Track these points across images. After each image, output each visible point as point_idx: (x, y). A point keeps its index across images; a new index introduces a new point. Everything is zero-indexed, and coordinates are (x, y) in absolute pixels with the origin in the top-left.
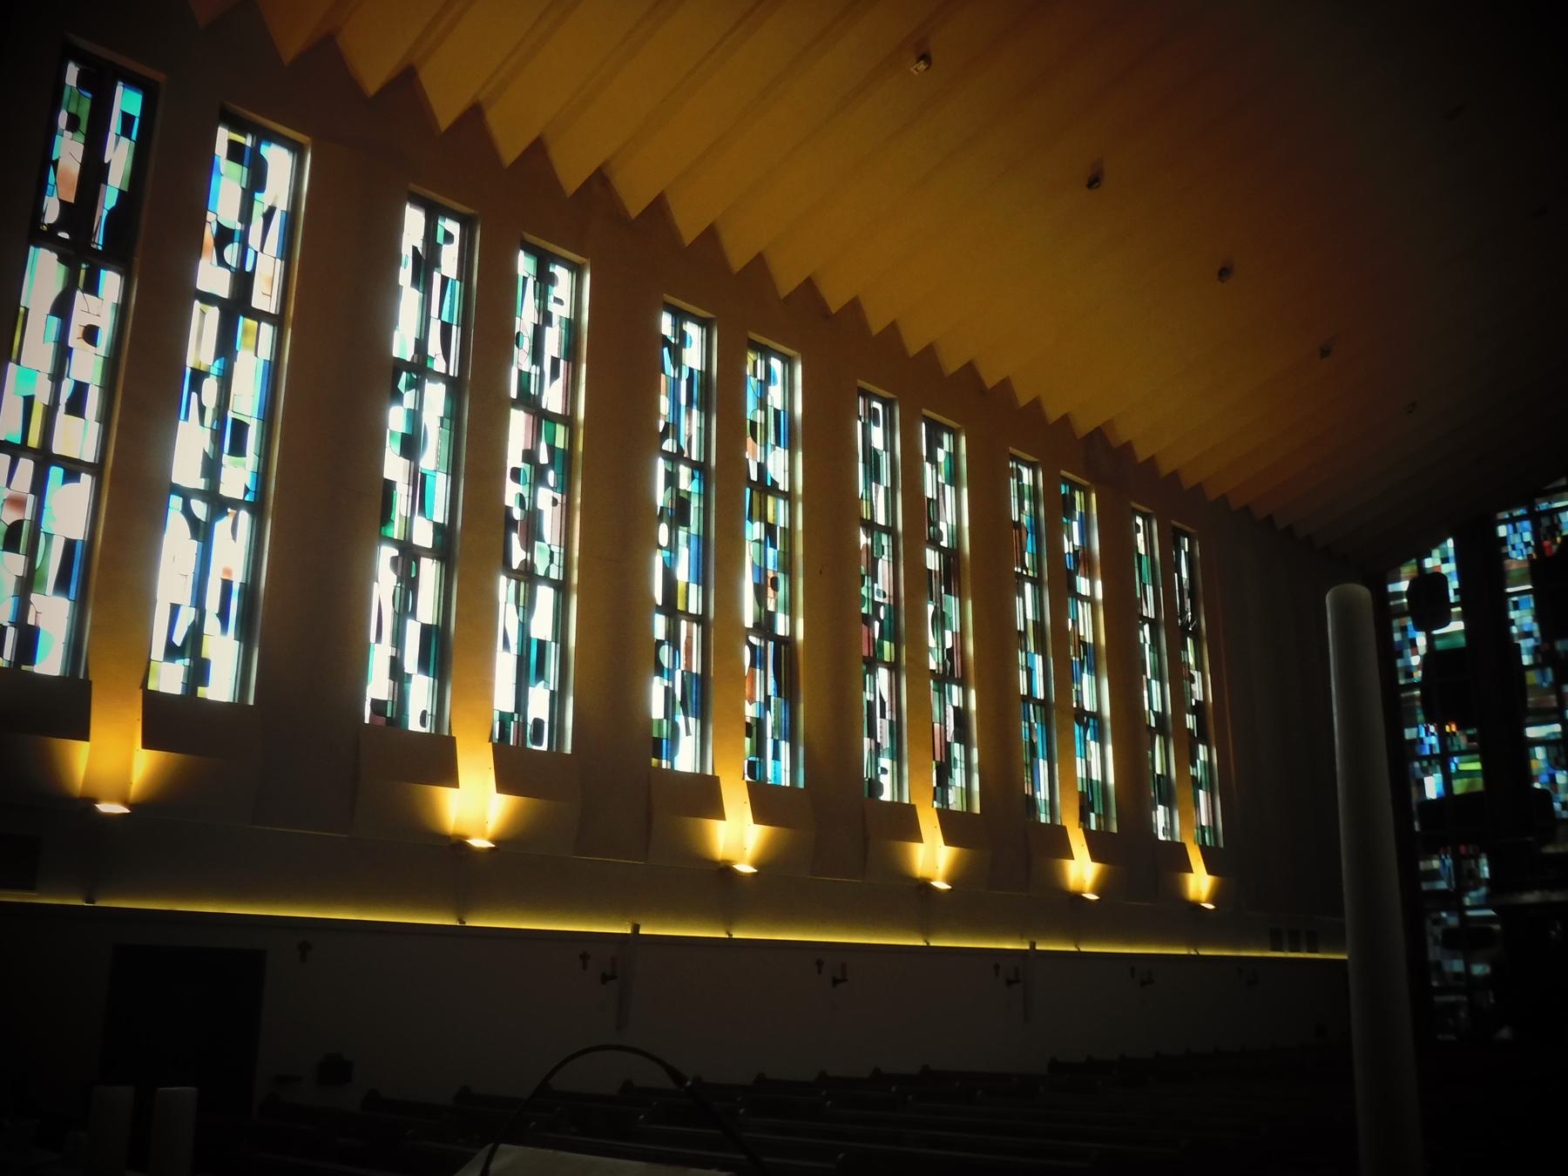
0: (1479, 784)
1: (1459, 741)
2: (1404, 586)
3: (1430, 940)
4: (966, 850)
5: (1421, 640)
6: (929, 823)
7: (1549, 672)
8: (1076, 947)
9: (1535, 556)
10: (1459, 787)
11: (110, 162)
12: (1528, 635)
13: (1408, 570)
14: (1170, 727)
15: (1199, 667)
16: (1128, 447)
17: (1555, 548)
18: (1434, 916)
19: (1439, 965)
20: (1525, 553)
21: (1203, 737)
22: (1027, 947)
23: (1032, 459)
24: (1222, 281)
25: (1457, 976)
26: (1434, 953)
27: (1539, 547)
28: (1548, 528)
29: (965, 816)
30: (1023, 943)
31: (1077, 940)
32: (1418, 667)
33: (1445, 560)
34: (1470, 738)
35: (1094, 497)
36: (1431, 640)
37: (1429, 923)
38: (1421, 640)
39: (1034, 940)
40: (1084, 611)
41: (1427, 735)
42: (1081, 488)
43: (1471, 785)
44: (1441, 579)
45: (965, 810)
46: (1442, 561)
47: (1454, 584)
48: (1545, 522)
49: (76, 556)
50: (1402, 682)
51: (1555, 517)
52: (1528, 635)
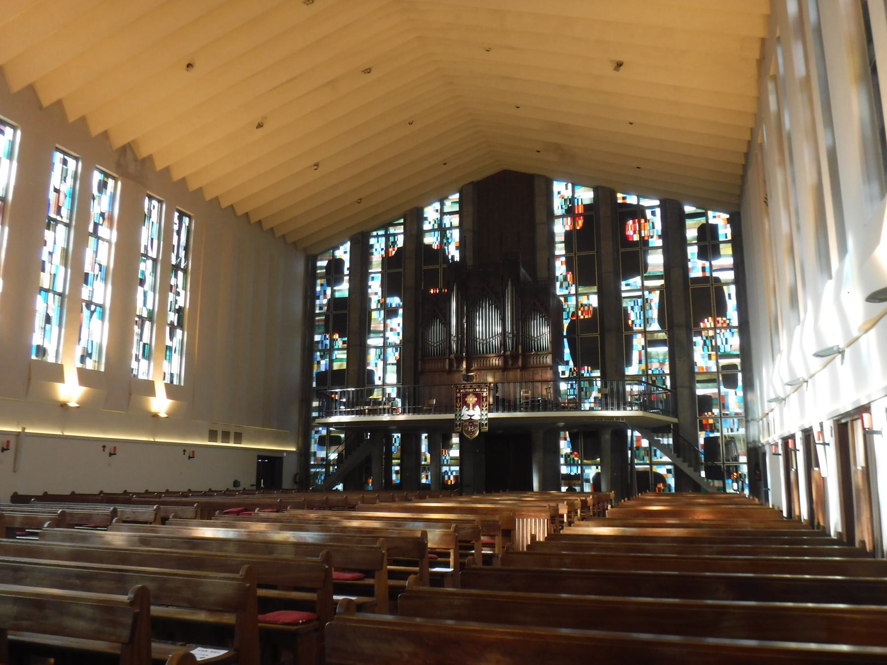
0: (344, 367)
1: (338, 343)
2: (324, 263)
3: (313, 441)
4: (179, 402)
5: (329, 291)
6: (160, 388)
7: (382, 312)
8: (62, 432)
9: (384, 256)
10: (336, 366)
11: (693, 268)
12: (376, 294)
13: (328, 255)
14: (155, 318)
15: (185, 288)
16: (149, 160)
17: (394, 253)
18: (316, 429)
19: (315, 453)
20: (381, 254)
21: (180, 325)
22: (20, 430)
23: (77, 155)
24: (188, 71)
25: (322, 459)
26: (314, 447)
27: (387, 251)
28: (392, 242)
29: (95, 373)
30: (18, 428)
31: (63, 429)
32: (325, 305)
33: (345, 252)
34: (344, 342)
35: (119, 183)
36: (333, 292)
37: (313, 432)
38: (329, 291)
39: (24, 426)
40: (103, 247)
41: (325, 339)
42: (114, 178)
43: (341, 365)
44: (340, 262)
45: (178, 384)
46: (343, 253)
47: (347, 265)
48: (391, 239)
49: (650, 416)
50: (317, 311)
51: (396, 237)
52: (376, 294)
